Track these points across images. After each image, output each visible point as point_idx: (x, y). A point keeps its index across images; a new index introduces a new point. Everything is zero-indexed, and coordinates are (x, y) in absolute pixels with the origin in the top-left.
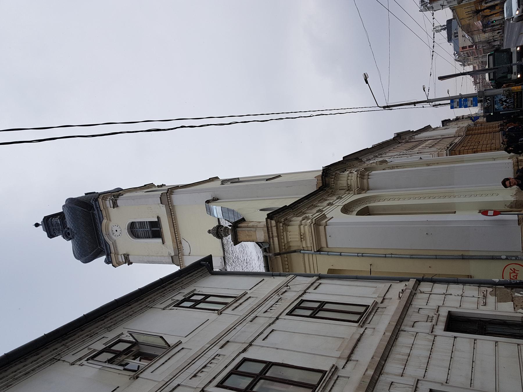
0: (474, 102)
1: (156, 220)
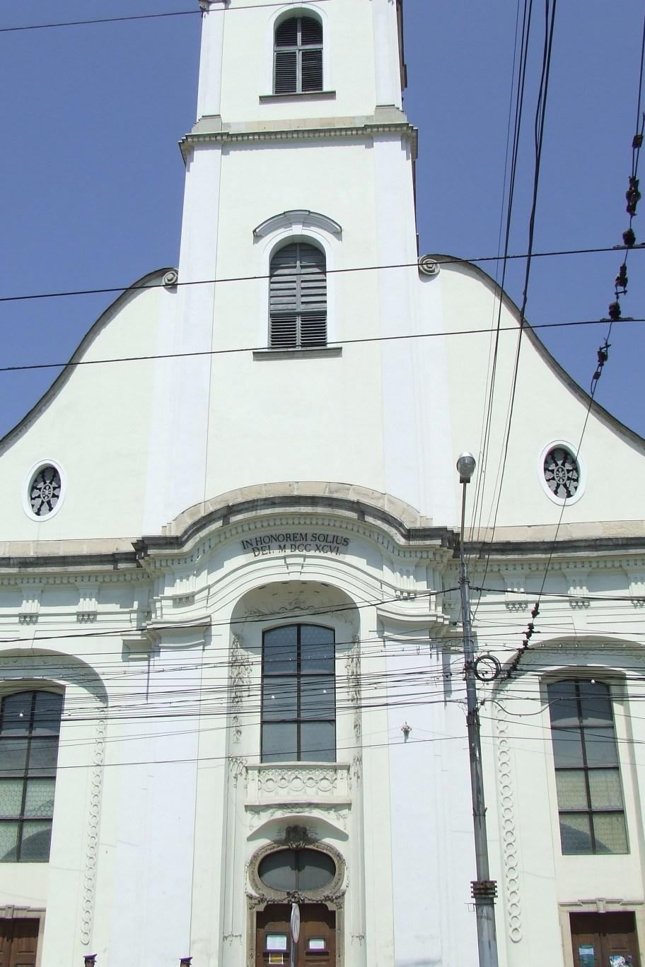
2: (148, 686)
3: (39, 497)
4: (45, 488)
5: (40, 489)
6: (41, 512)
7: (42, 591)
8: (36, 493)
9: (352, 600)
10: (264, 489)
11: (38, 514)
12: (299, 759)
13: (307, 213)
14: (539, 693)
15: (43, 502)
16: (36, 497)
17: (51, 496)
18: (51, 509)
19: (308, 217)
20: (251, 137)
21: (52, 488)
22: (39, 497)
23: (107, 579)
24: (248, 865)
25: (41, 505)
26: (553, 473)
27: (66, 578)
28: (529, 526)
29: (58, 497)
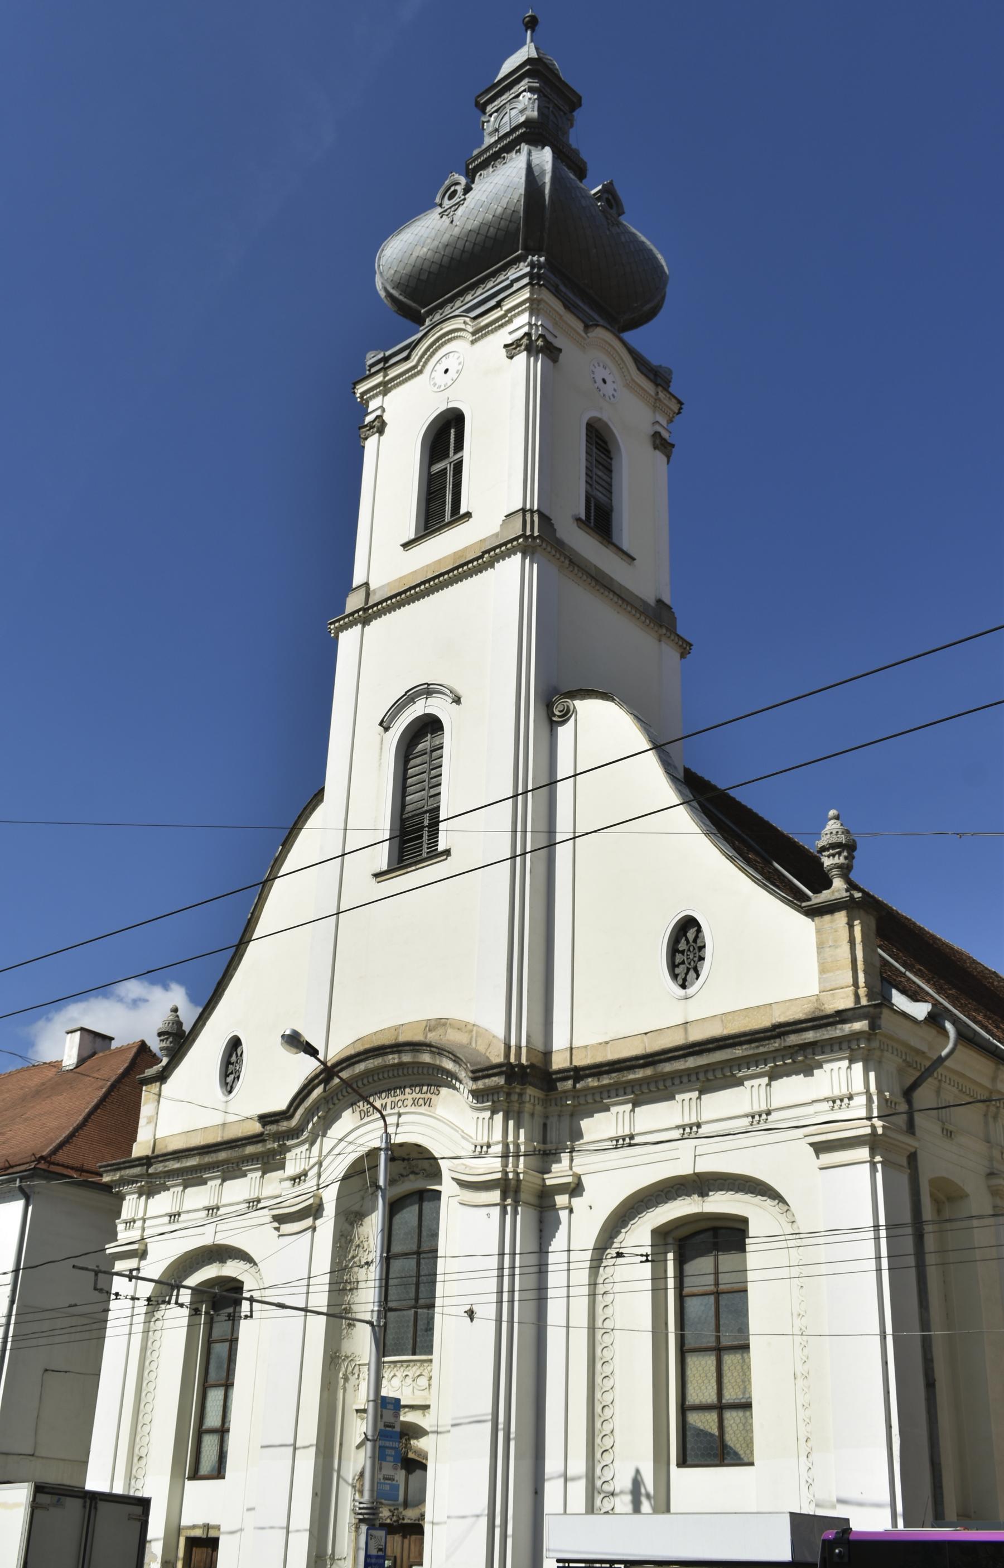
0: (387, 1488)
1: (463, 511)
2: (569, 1251)
3: (683, 963)
4: (689, 950)
5: (682, 952)
6: (687, 983)
7: (559, 1116)
8: (679, 958)
9: (433, 1154)
10: (374, 1038)
11: (683, 986)
12: (414, 1354)
13: (426, 686)
14: (650, 1247)
15: (688, 970)
16: (679, 964)
17: (696, 959)
18: (698, 976)
19: (428, 691)
20: (356, 615)
21: (696, 948)
22: (683, 963)
23: (710, 1076)
24: (357, 1478)
25: (687, 974)
26: (683, 955)
27: (670, 1080)
28: (646, 1034)
29: (703, 959)
